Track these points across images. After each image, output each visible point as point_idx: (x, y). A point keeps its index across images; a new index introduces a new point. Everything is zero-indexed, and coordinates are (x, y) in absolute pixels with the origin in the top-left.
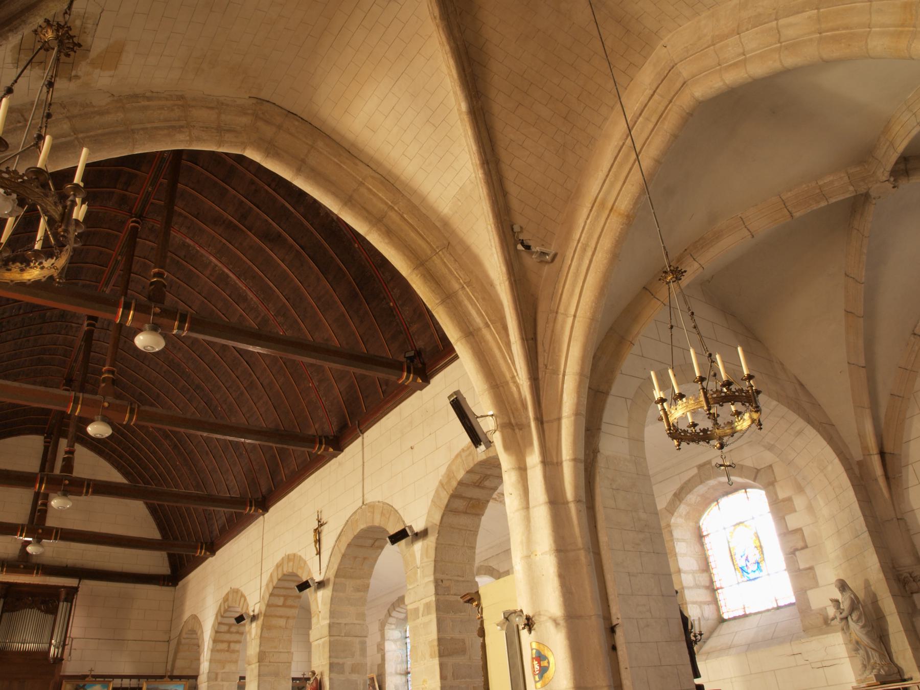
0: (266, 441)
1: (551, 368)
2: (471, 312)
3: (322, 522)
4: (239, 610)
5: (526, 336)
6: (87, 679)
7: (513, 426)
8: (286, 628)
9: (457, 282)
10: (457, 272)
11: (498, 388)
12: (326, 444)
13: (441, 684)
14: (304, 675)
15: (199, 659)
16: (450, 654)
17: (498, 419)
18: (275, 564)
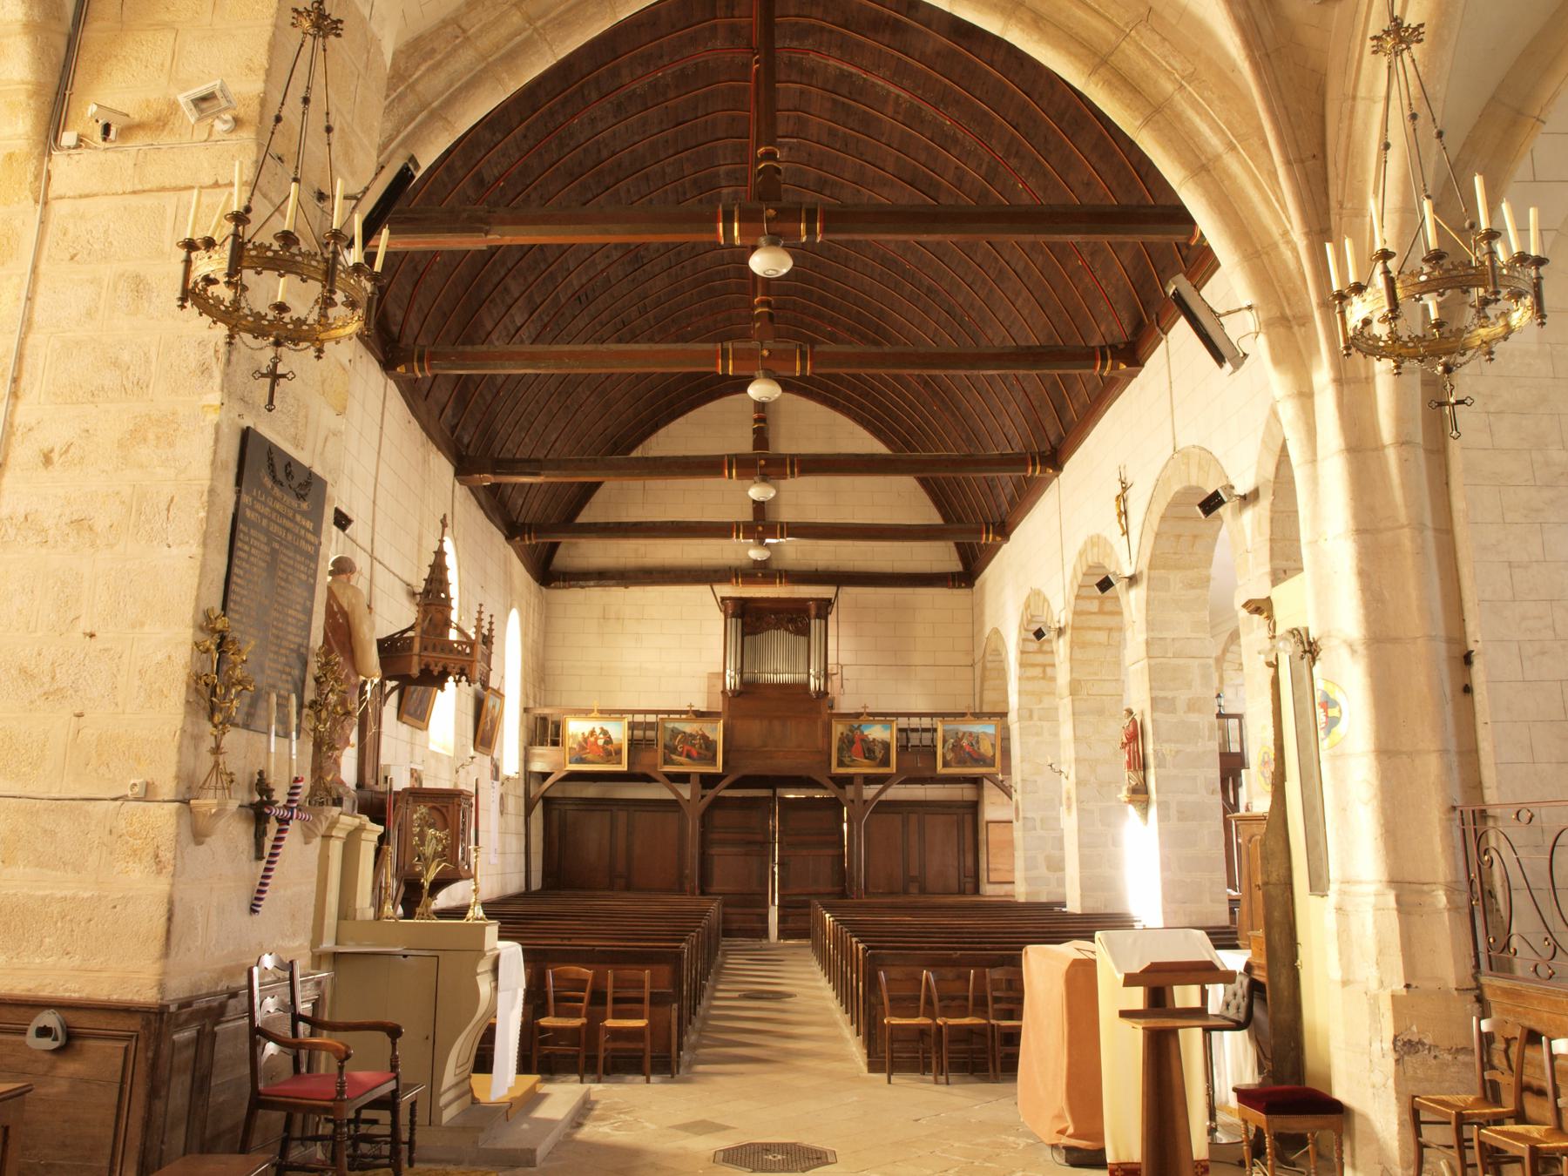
1: (1350, 205)
2: (1202, 129)
6: (861, 718)
7: (1289, 321)
9: (1169, 79)
10: (1167, 62)
11: (1259, 257)
12: (1112, 358)
17: (1260, 313)
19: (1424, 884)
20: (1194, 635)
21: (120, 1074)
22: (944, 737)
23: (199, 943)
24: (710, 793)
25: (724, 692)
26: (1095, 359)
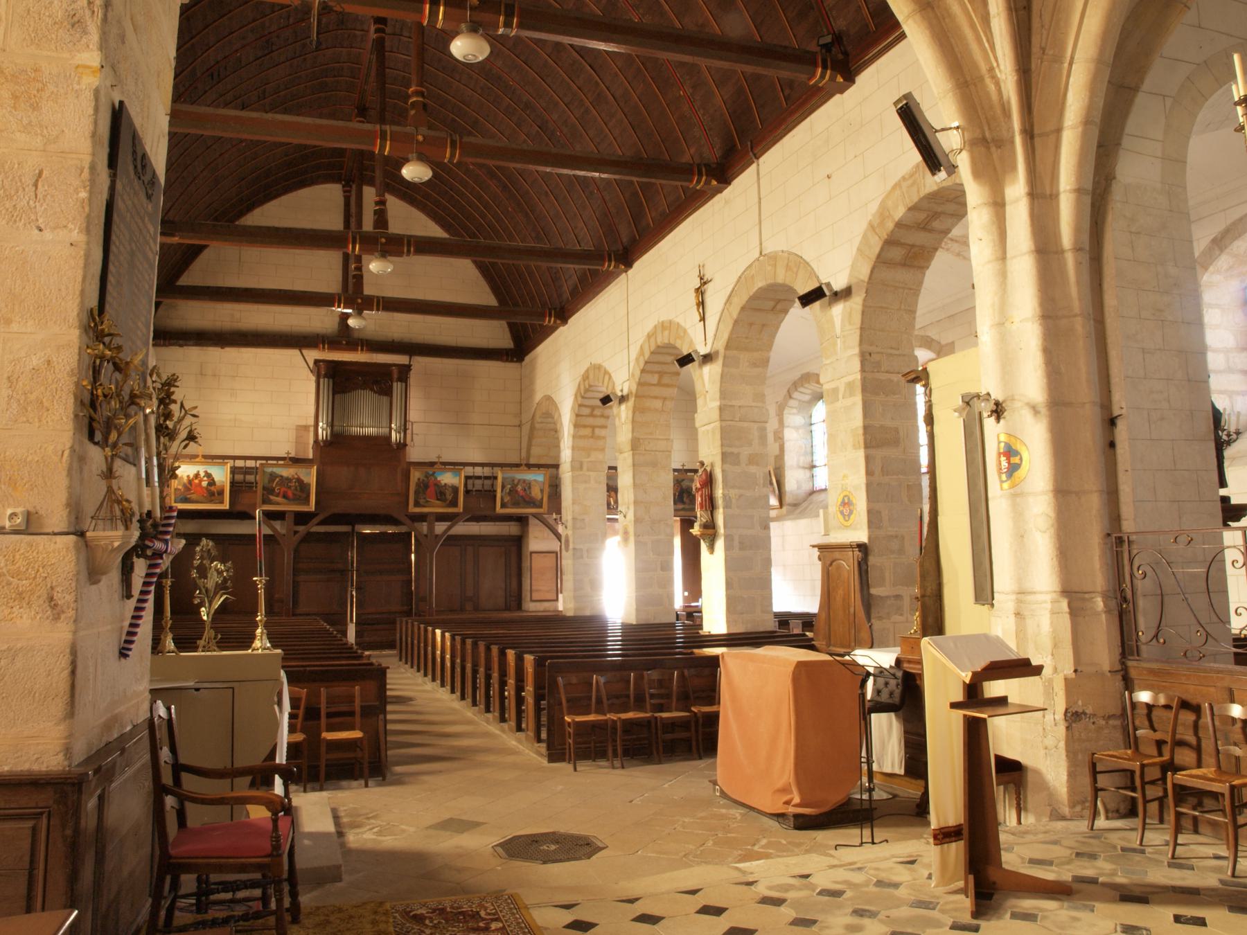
0: (628, 175)
3: (705, 280)
4: (604, 389)
5: (1015, 4)
6: (436, 466)
8: (663, 411)
12: (707, 175)
13: (867, 480)
14: (683, 465)
15: (558, 446)
16: (878, 446)
17: (966, 133)
19: (1086, 593)
20: (754, 404)
21: (27, 859)
22: (503, 483)
23: (90, 697)
24: (301, 528)
25: (316, 441)
26: (693, 174)
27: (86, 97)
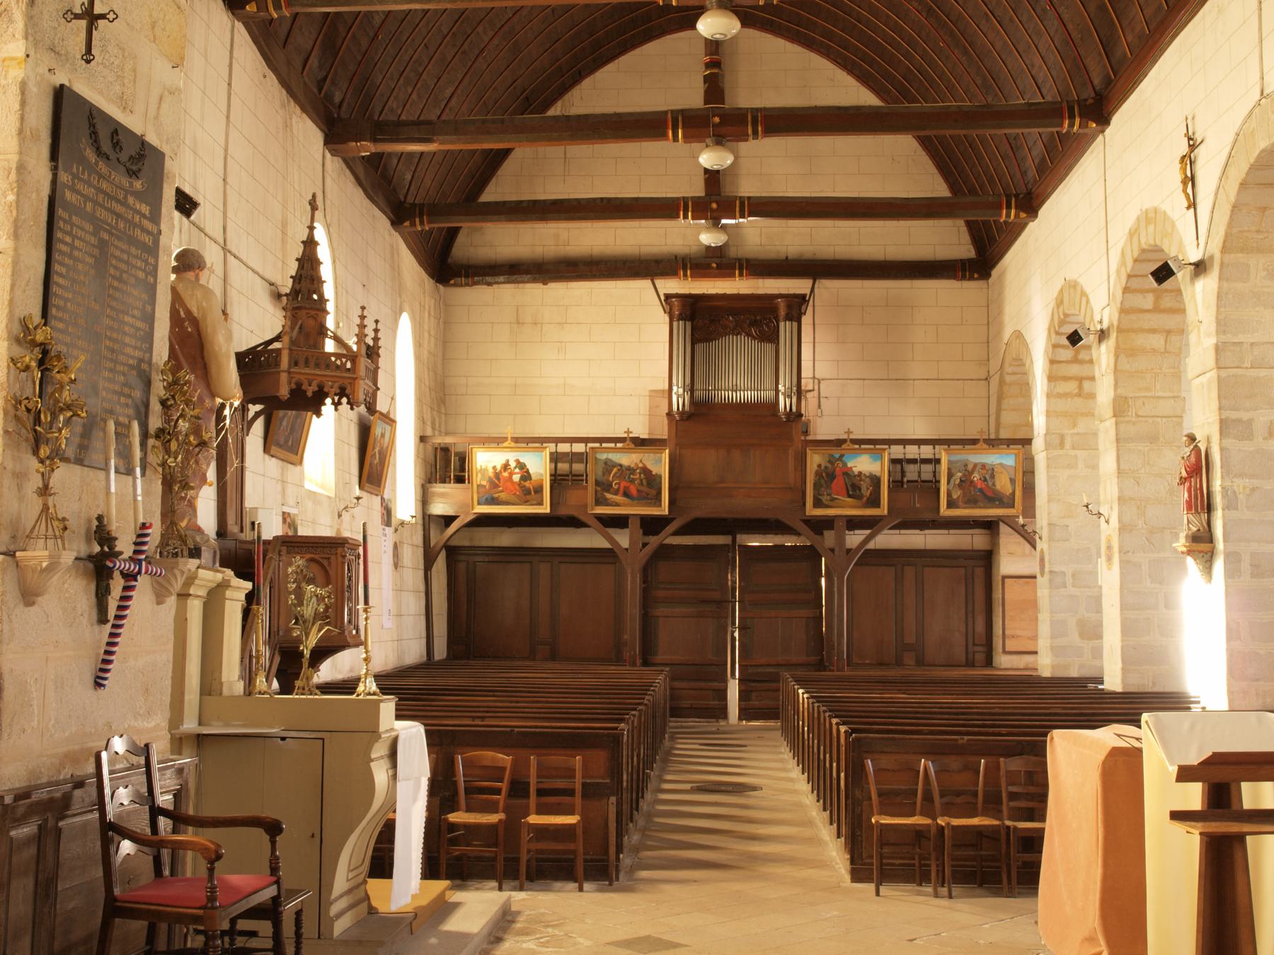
6: (844, 446)
8: (1166, 351)
18: (1127, 231)
22: (949, 469)
24: (654, 541)
27: (12, 92)
